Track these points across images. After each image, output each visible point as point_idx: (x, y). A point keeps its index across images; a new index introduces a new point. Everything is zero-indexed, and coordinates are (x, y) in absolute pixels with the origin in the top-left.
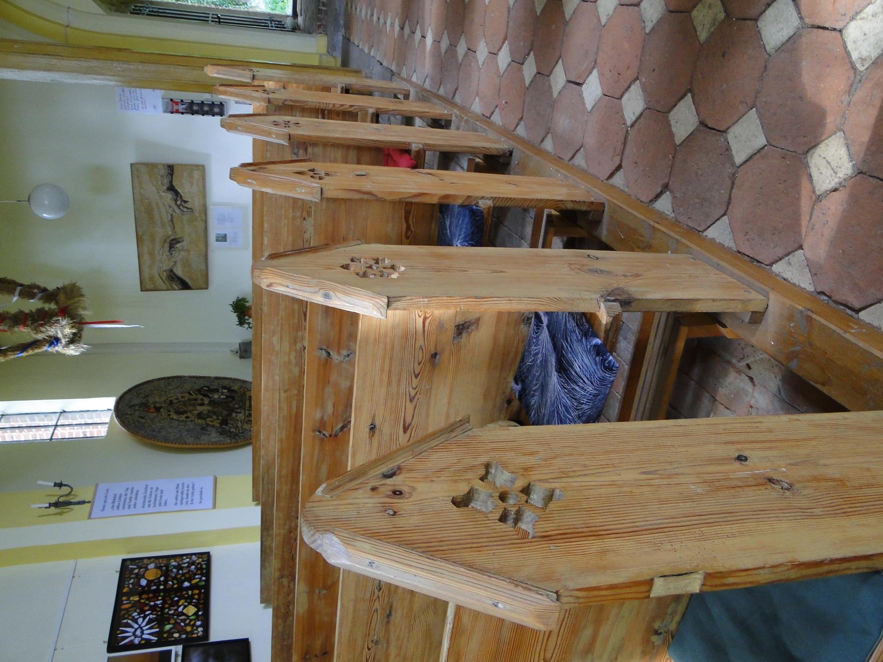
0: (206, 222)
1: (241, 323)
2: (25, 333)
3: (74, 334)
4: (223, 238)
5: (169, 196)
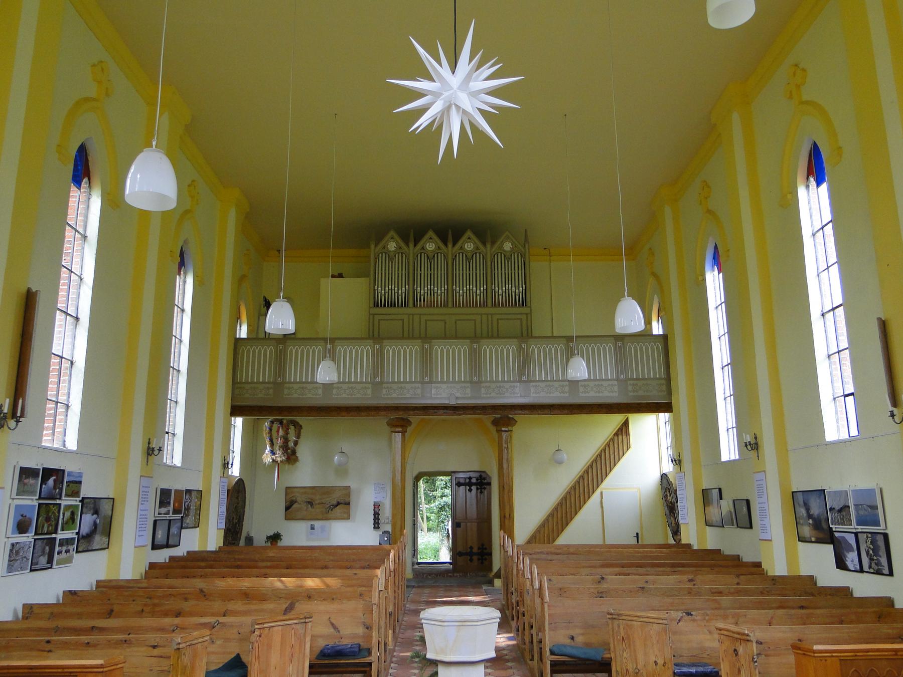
0: (322, 519)
1: (268, 538)
2: (279, 442)
4: (312, 528)
5: (335, 503)
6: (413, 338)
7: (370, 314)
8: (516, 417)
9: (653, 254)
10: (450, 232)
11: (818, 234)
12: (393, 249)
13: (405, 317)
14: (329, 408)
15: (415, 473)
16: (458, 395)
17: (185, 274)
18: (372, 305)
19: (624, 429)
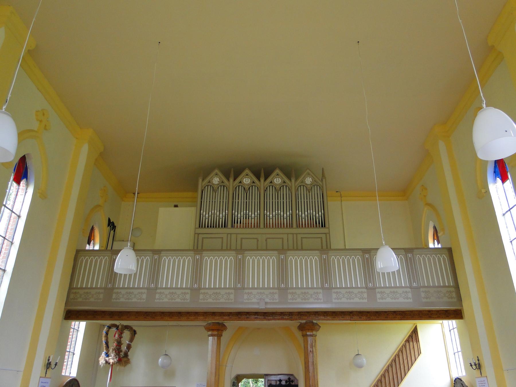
2: (113, 345)
3: (110, 363)
6: (230, 250)
7: (195, 234)
8: (320, 322)
9: (426, 189)
10: (262, 169)
11: (506, 214)
12: (217, 183)
13: (225, 236)
14: (154, 313)
15: (234, 375)
16: (267, 300)
17: (27, 185)
18: (197, 226)
19: (414, 336)
